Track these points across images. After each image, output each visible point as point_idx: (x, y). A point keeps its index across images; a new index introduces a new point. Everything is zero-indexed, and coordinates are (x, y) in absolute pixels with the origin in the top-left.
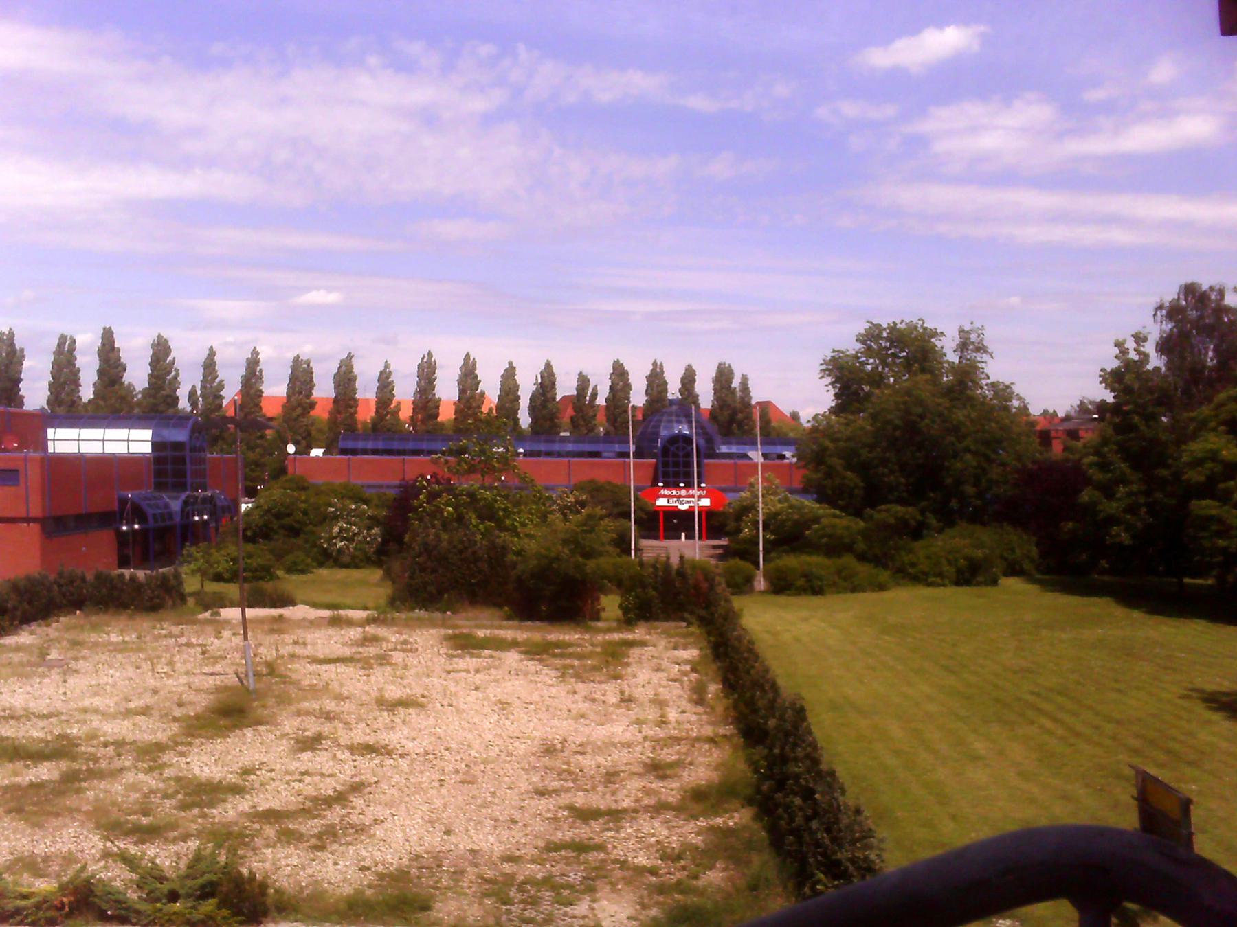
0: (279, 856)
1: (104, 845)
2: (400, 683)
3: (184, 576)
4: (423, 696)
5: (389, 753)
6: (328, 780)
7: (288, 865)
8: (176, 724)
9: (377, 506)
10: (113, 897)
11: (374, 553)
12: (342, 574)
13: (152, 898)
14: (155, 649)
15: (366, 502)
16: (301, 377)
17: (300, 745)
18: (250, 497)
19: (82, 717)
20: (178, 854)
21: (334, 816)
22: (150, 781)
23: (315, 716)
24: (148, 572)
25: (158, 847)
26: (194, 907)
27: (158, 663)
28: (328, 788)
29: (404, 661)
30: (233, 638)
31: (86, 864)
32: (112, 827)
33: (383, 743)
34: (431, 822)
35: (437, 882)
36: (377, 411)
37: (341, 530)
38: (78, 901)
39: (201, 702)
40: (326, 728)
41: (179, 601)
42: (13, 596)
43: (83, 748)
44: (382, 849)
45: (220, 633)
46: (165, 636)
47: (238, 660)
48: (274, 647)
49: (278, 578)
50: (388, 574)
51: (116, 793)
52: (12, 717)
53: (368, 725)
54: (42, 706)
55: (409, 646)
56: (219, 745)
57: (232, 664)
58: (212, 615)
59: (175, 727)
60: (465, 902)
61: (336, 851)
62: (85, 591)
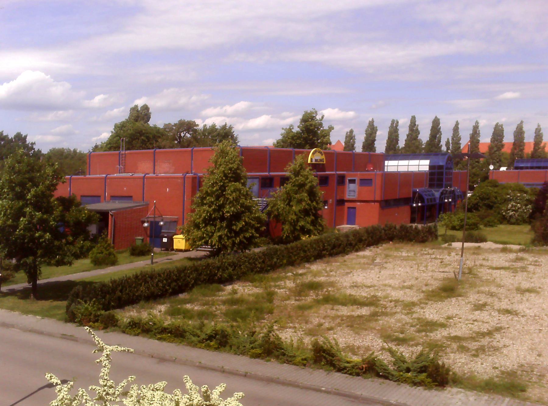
0: (456, 358)
1: (383, 345)
2: (529, 281)
3: (438, 227)
4: (540, 288)
5: (517, 314)
6: (485, 325)
7: (460, 362)
8: (423, 294)
9: (531, 195)
10: (383, 367)
11: (527, 217)
12: (510, 228)
13: (399, 370)
14: (420, 260)
15: (526, 192)
16: (498, 133)
17: (476, 308)
18: (470, 191)
19: (384, 288)
20: (413, 353)
21: (485, 341)
22: (407, 319)
23: (486, 294)
24: (423, 225)
25: (405, 348)
26: (416, 376)
27: (420, 266)
28: (485, 328)
29: (534, 270)
30: (456, 256)
31: (374, 352)
32: (387, 338)
33: (515, 309)
34: (532, 349)
35: (530, 379)
36: (534, 148)
37: (512, 206)
38: (369, 367)
39: (435, 285)
40: (489, 300)
41: (434, 239)
42: (366, 235)
43: (381, 302)
44: (505, 359)
45: (450, 253)
46: (426, 254)
47: (456, 266)
48: (473, 261)
49: (480, 229)
50: (533, 228)
51: (391, 323)
52: (356, 286)
53: (509, 300)
54: (368, 282)
55: (538, 264)
56: (439, 305)
57: (453, 268)
58: (448, 245)
59: (422, 295)
60: (544, 391)
61: (483, 358)
62: (395, 233)
